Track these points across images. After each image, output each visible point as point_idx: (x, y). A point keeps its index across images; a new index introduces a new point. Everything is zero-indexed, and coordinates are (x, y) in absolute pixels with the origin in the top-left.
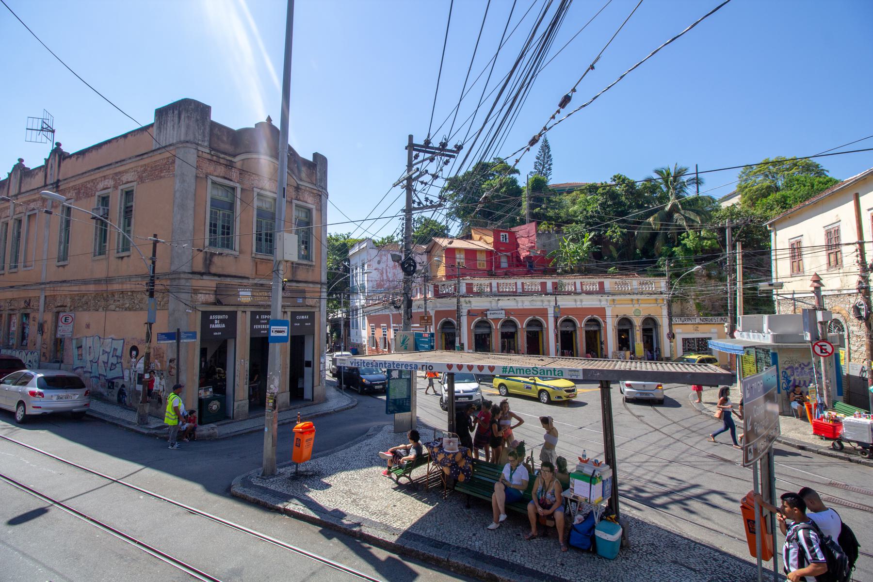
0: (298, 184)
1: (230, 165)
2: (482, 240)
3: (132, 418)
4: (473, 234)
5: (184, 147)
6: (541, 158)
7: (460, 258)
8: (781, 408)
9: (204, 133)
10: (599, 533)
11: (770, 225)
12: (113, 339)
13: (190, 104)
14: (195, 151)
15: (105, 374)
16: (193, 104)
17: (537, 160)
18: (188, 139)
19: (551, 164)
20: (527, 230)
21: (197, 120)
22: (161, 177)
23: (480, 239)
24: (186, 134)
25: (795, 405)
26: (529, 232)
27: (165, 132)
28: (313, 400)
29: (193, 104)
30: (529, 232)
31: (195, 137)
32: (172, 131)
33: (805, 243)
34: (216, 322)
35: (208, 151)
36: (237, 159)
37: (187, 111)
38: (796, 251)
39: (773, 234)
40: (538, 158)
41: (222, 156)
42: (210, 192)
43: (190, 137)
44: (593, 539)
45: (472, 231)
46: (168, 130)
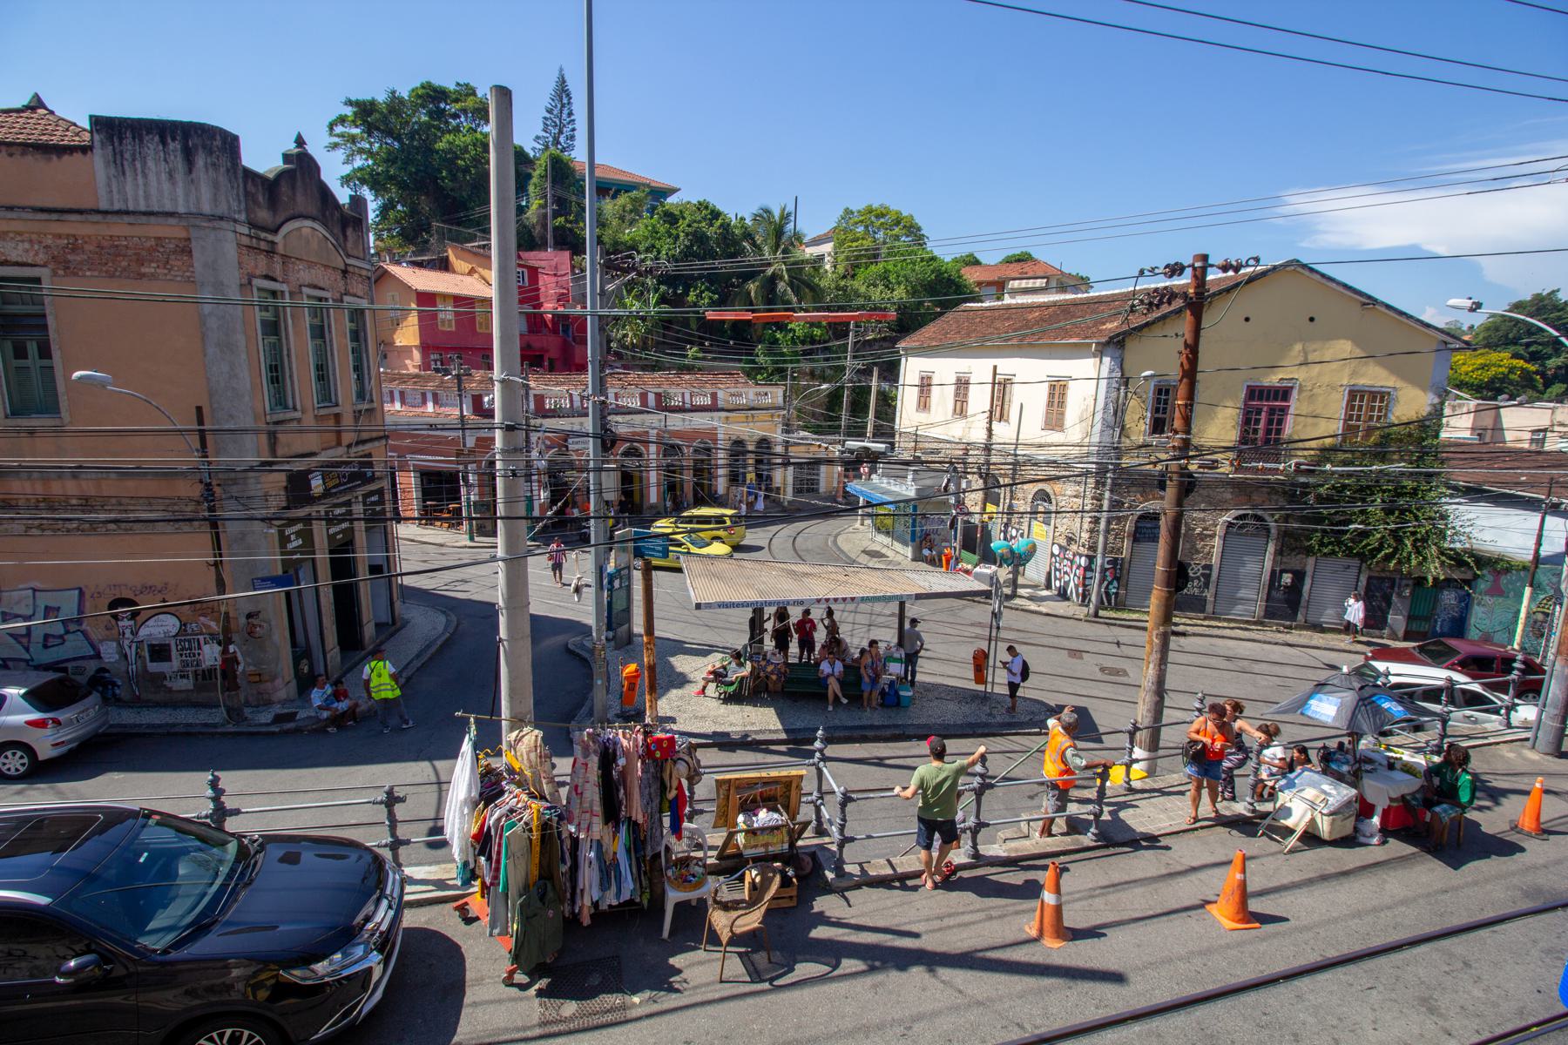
0: (346, 265)
1: (271, 251)
2: (476, 276)
3: (218, 716)
4: (452, 258)
5: (214, 228)
6: (555, 112)
7: (446, 313)
8: (914, 552)
9: (238, 195)
10: (902, 693)
11: (904, 349)
12: (35, 590)
13: (213, 138)
14: (231, 235)
15: (28, 657)
16: (218, 137)
17: (548, 115)
18: (219, 212)
19: (573, 130)
20: (553, 263)
21: (228, 171)
22: (142, 276)
23: (471, 272)
24: (215, 200)
25: (926, 552)
26: (556, 268)
27: (140, 180)
28: (394, 623)
29: (218, 137)
30: (556, 268)
31: (229, 208)
32: (166, 186)
33: (935, 381)
34: (293, 537)
35: (246, 231)
36: (278, 238)
37: (211, 152)
38: (925, 385)
39: (903, 360)
40: (550, 111)
41: (263, 235)
42: (259, 315)
43: (222, 209)
44: (898, 697)
45: (450, 251)
46: (152, 177)
